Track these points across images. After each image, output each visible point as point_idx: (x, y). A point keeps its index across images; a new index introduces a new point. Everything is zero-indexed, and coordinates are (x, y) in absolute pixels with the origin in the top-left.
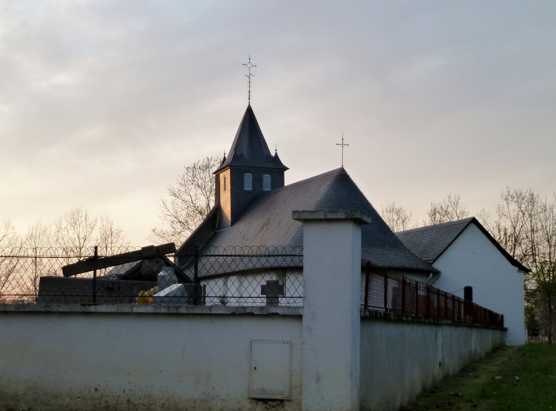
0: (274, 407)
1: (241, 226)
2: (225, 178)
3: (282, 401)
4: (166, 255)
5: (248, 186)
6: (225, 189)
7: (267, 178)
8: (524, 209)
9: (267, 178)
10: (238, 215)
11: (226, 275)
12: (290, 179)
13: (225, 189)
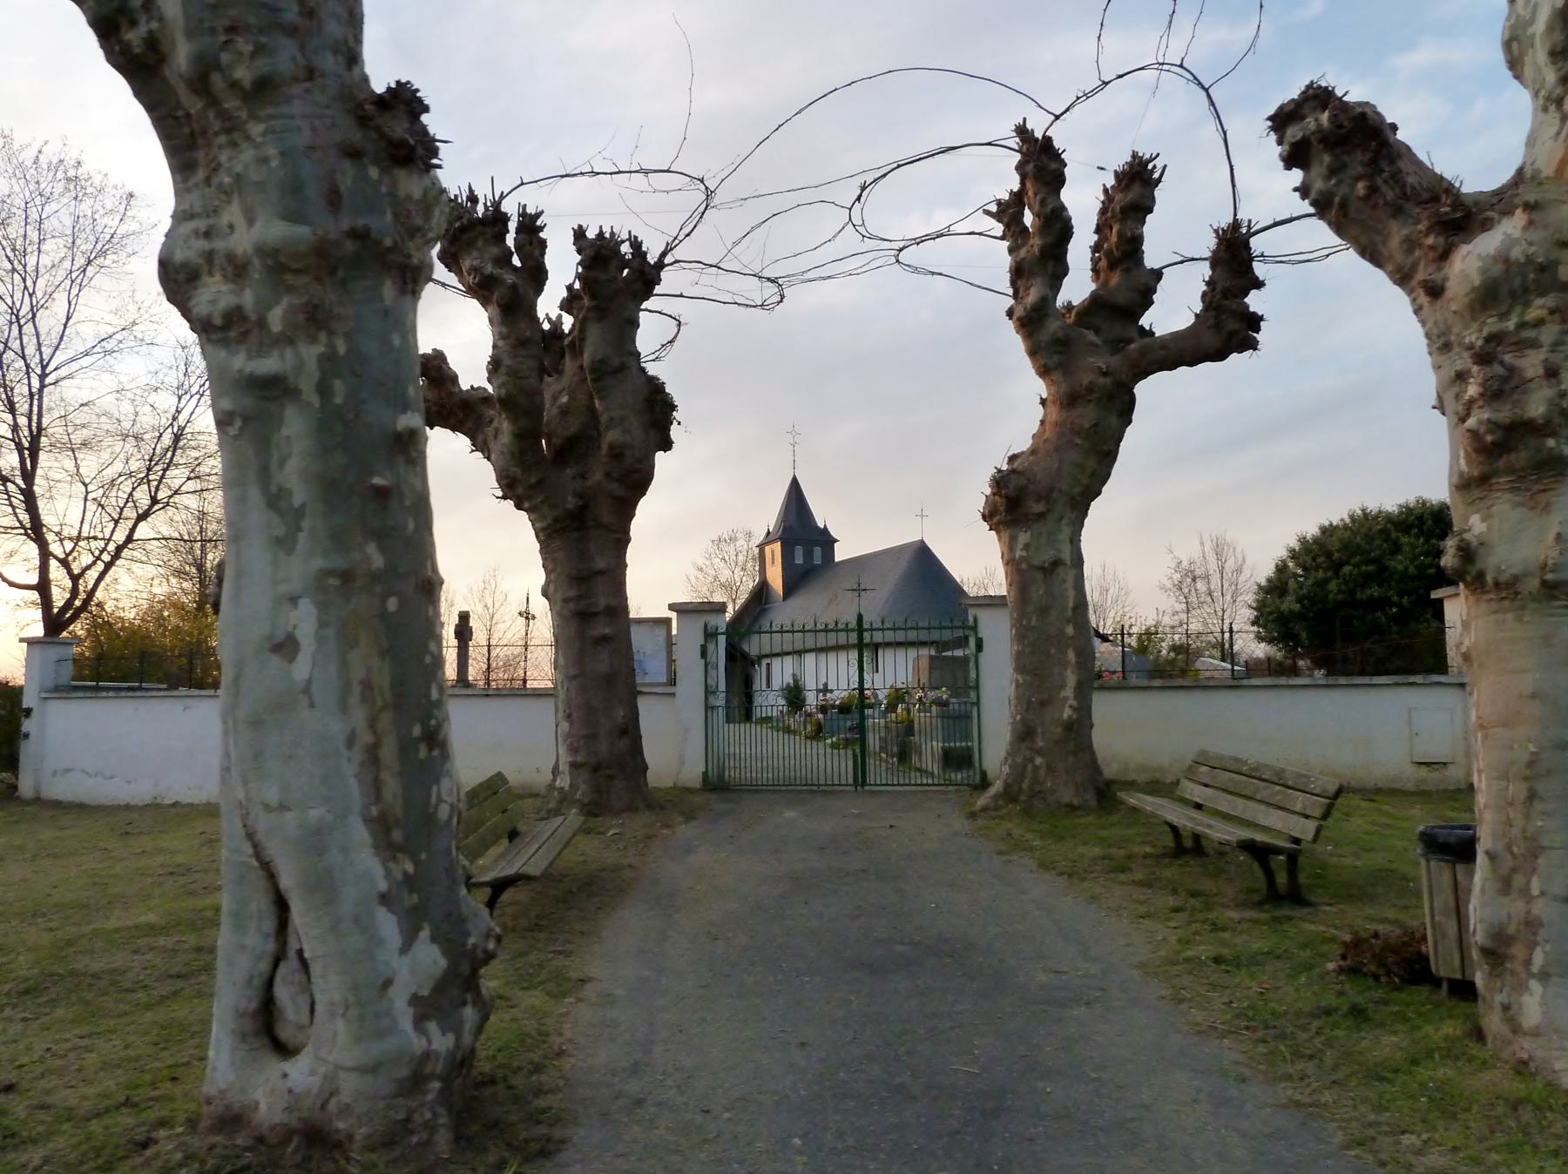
0: (1437, 769)
1: (791, 602)
2: (773, 552)
3: (1445, 764)
4: (1435, 595)
5: (799, 560)
6: (773, 563)
7: (817, 551)
8: (1187, 591)
9: (817, 551)
10: (790, 588)
11: (800, 653)
12: (841, 553)
13: (773, 563)
